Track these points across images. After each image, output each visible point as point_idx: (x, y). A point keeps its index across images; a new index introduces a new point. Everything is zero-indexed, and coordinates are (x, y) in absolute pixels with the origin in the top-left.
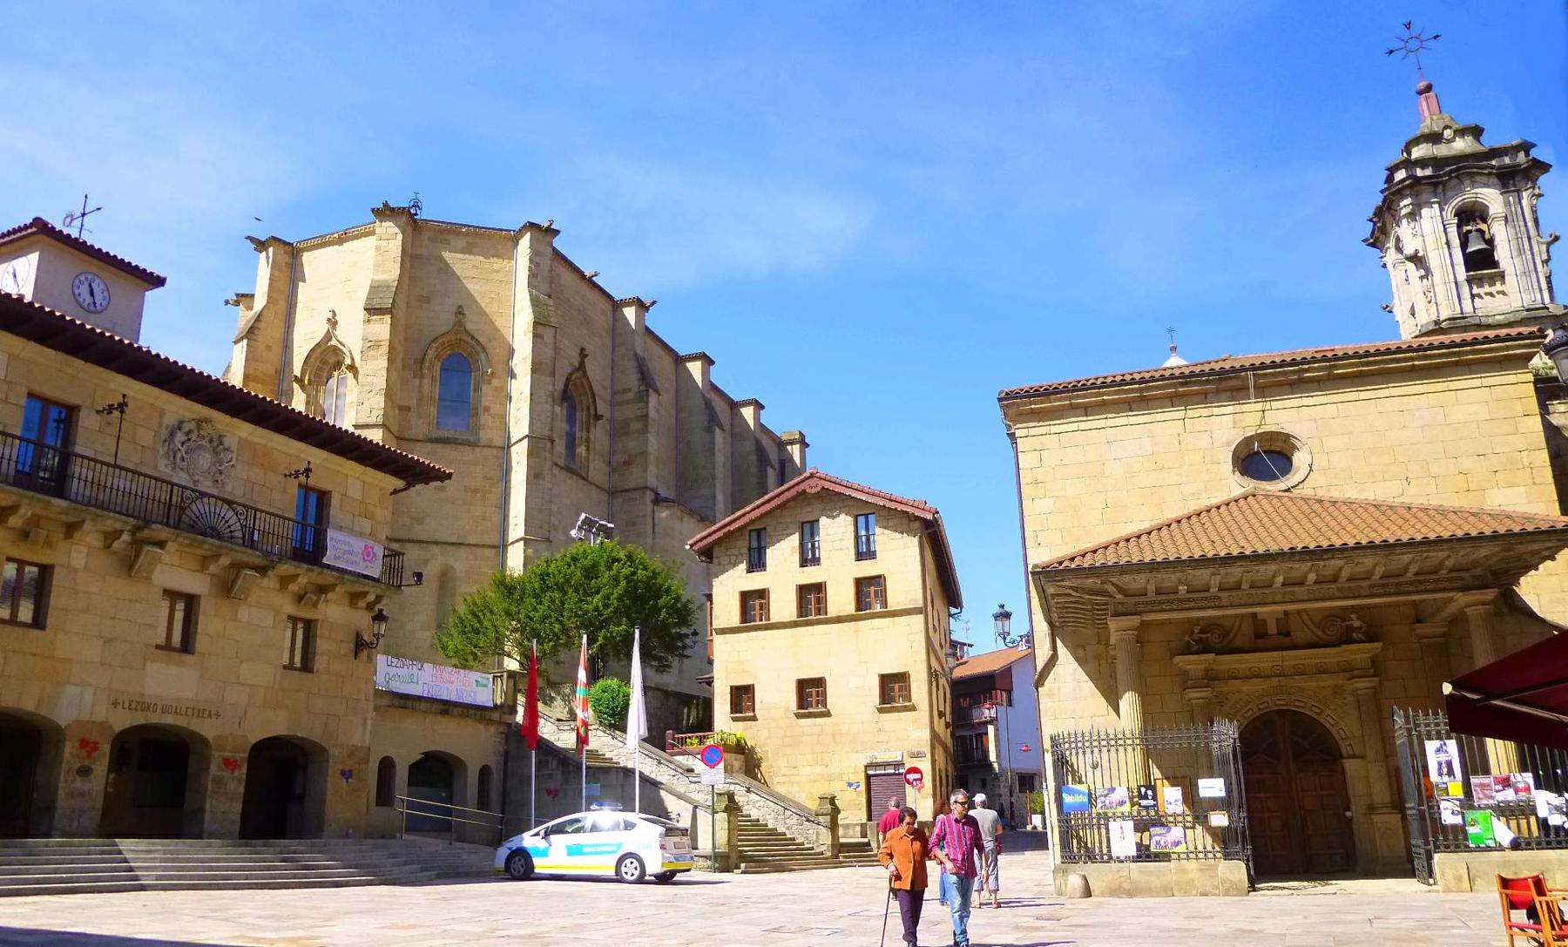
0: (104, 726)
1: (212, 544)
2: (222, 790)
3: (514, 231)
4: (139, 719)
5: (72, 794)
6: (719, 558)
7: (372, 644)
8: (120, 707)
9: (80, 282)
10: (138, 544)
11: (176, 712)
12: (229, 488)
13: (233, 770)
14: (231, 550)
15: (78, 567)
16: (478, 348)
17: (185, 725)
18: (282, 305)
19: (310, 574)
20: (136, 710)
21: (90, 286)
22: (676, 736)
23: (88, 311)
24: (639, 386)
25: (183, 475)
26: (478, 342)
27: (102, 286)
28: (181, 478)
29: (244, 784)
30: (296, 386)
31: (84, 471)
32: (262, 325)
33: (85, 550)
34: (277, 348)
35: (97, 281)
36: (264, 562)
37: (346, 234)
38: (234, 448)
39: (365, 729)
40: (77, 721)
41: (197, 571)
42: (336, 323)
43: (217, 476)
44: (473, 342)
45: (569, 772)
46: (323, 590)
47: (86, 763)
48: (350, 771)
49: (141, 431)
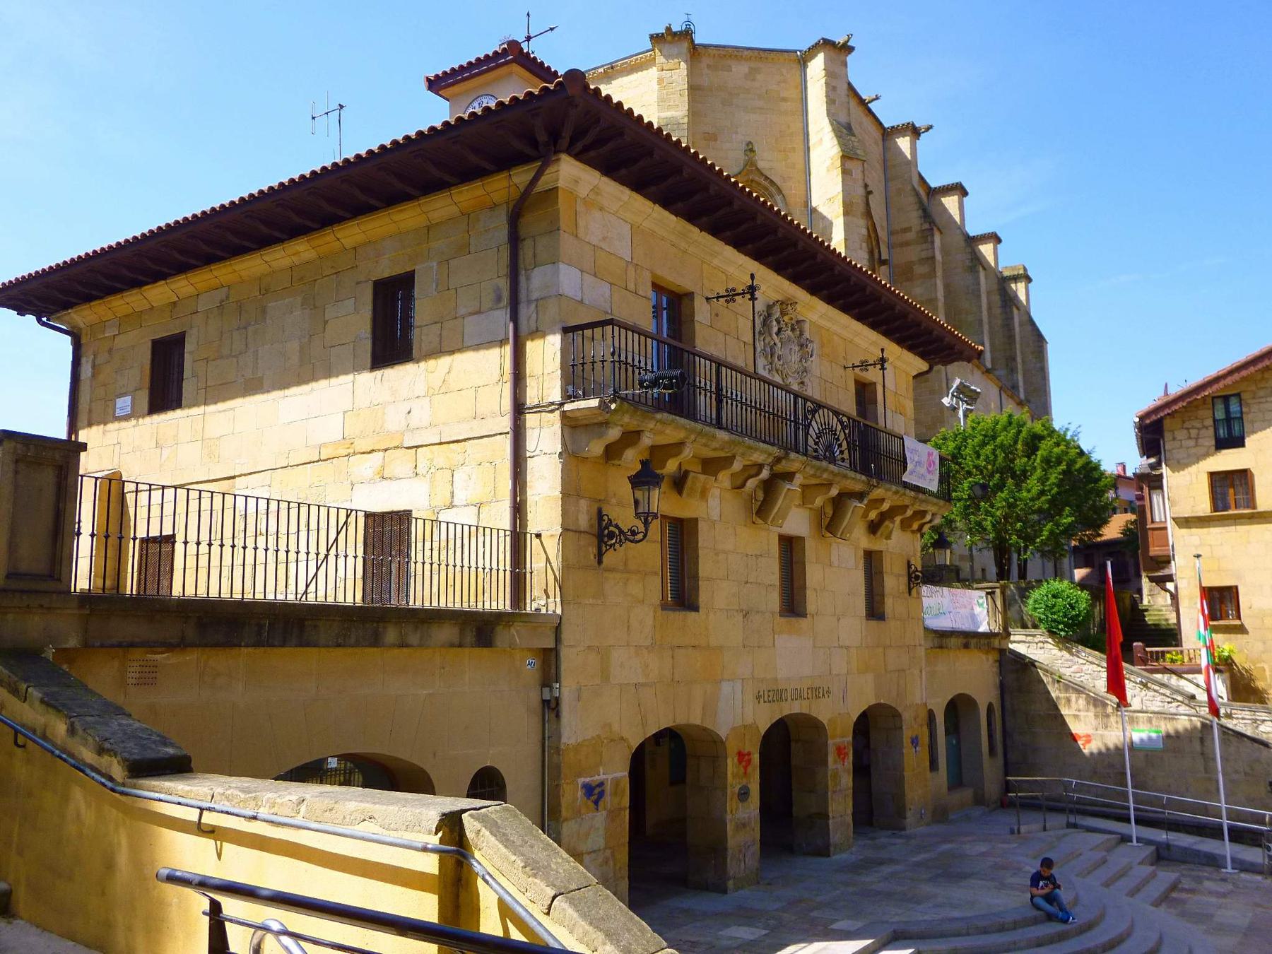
3: (800, 51)
6: (1173, 431)
7: (634, 533)
16: (773, 190)
20: (774, 701)
22: (1148, 649)
24: (921, 224)
26: (772, 182)
37: (612, 68)
44: (766, 183)
45: (1108, 716)
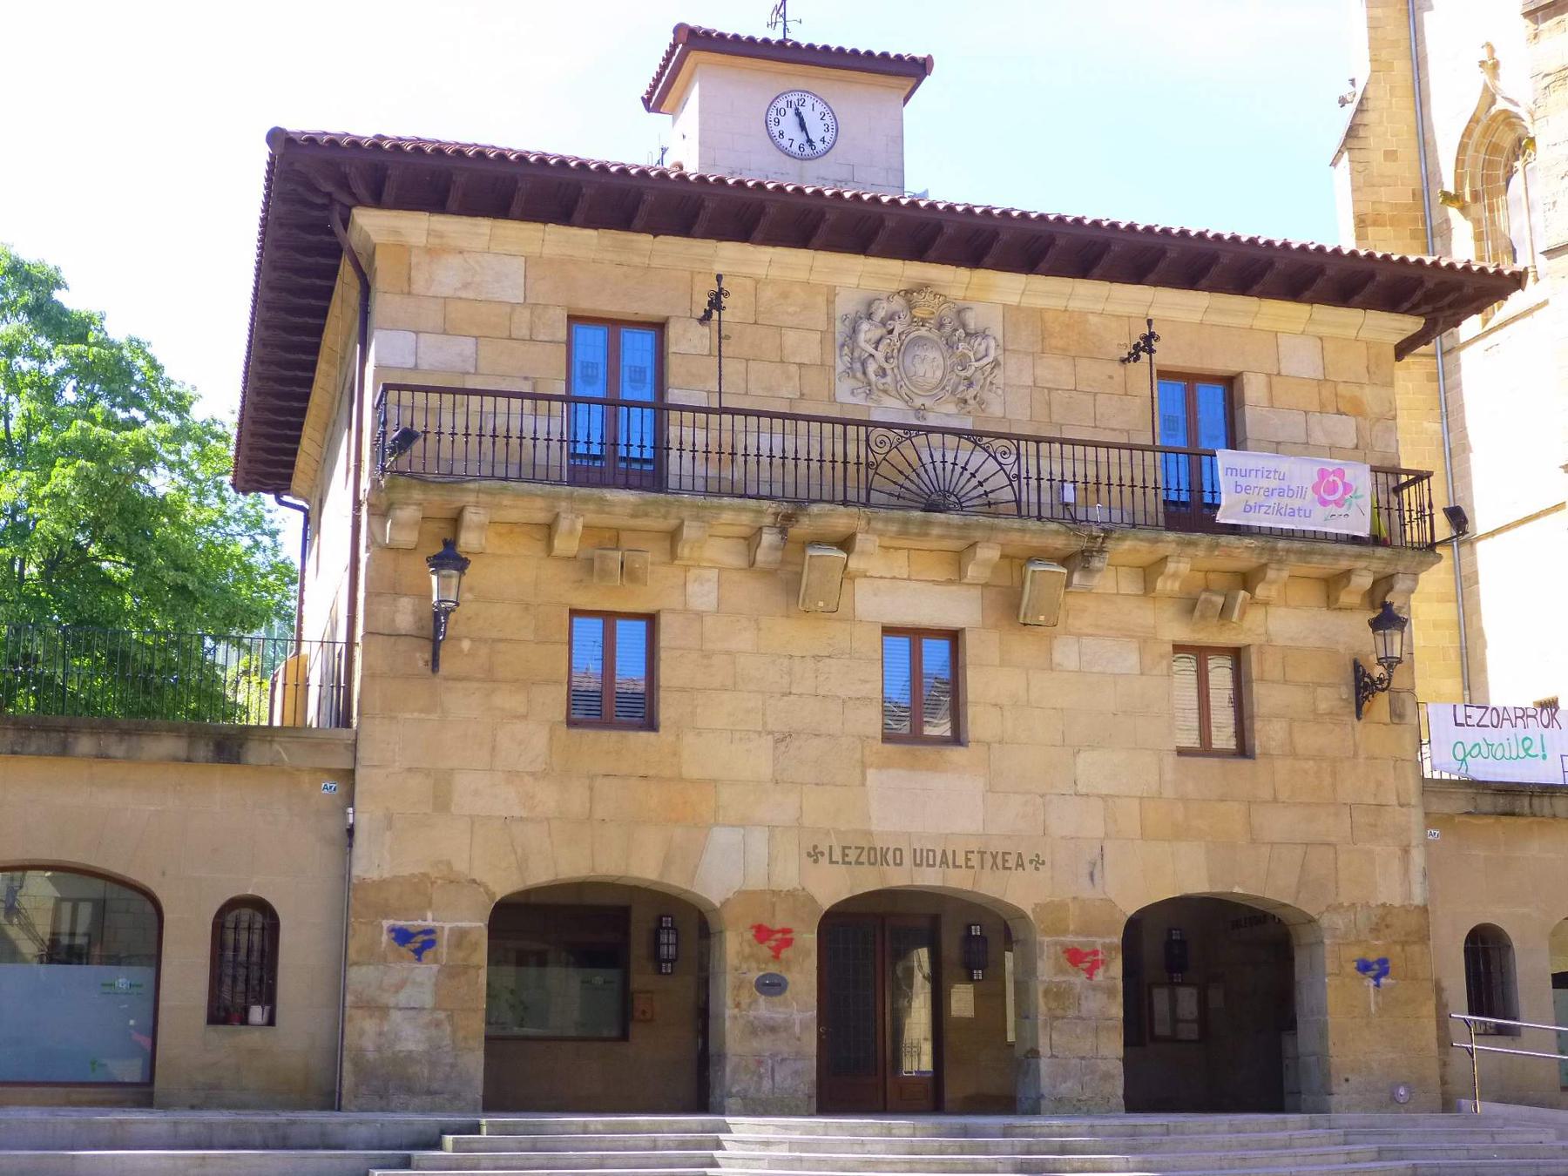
0: (798, 899)
1: (948, 525)
2: (1071, 1013)
4: (869, 881)
5: (755, 1029)
8: (824, 861)
9: (779, 112)
10: (795, 548)
11: (944, 862)
12: (996, 409)
13: (1090, 972)
14: (992, 528)
15: (703, 608)
17: (968, 886)
18: (1402, 68)
19: (1190, 551)
20: (858, 863)
21: (798, 114)
23: (802, 159)
25: (890, 402)
27: (819, 108)
28: (890, 409)
29: (1120, 999)
30: (1453, 212)
31: (701, 436)
32: (1370, 118)
33: (714, 574)
34: (1409, 152)
35: (809, 101)
36: (1076, 545)
38: (997, 330)
39: (1406, 871)
40: (739, 893)
41: (950, 582)
42: (1496, 65)
43: (964, 389)
46: (1246, 580)
47: (773, 968)
48: (1383, 962)
49: (791, 338)
